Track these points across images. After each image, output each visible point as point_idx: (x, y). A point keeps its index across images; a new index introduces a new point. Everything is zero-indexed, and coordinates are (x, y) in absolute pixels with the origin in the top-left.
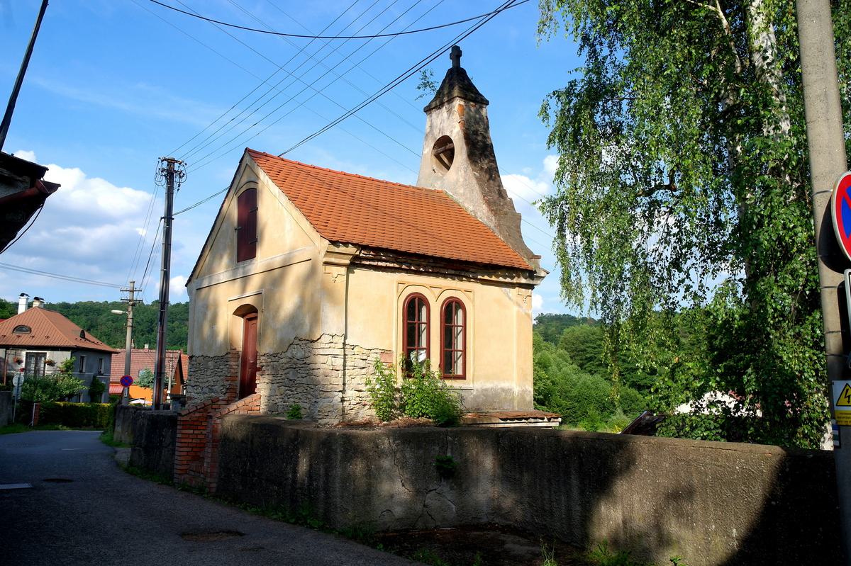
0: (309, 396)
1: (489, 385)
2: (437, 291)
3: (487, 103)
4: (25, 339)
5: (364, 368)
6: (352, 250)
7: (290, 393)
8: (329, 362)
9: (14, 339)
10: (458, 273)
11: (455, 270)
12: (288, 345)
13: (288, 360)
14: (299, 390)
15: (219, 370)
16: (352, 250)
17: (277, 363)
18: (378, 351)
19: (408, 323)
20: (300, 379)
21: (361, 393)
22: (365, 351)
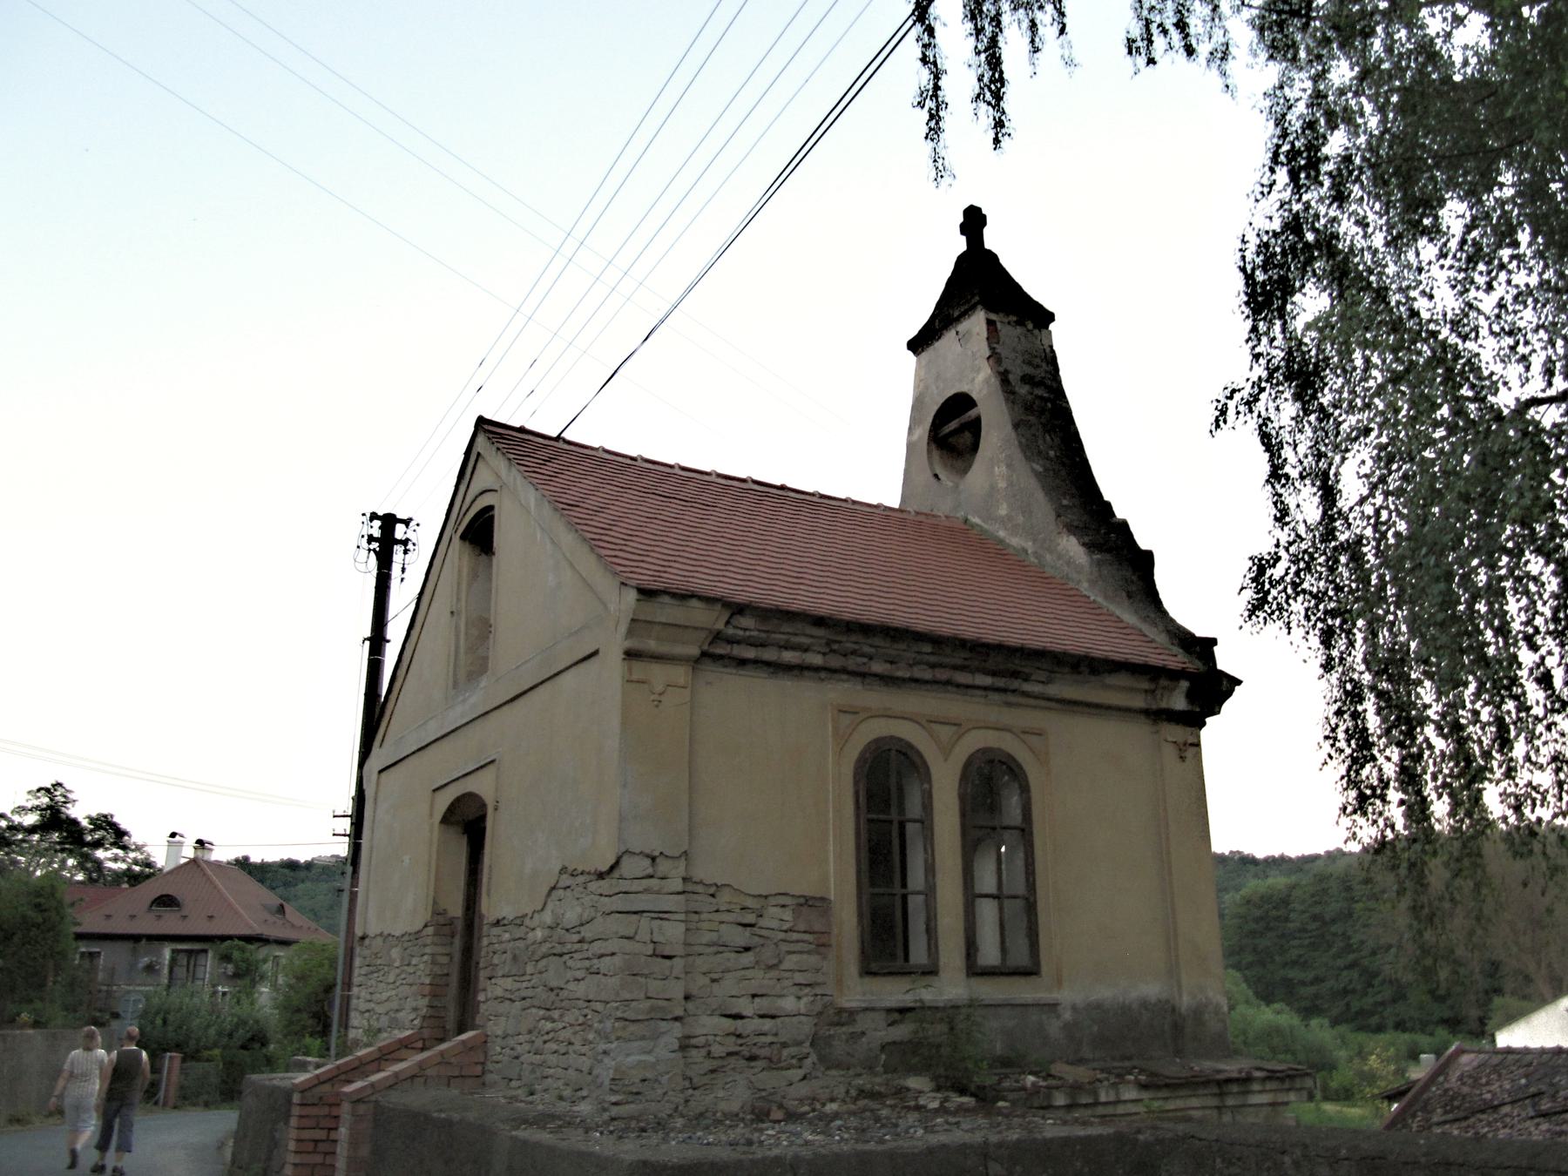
0: (591, 1036)
1: (1105, 993)
2: (945, 732)
3: (1050, 317)
4: (170, 923)
5: (747, 949)
6: (714, 619)
7: (549, 1026)
8: (644, 935)
9: (148, 924)
10: (1000, 682)
11: (994, 674)
12: (545, 890)
13: (547, 932)
14: (569, 1018)
15: (411, 969)
16: (714, 619)
17: (520, 944)
18: (787, 900)
19: (870, 821)
20: (572, 986)
21: (739, 1022)
22: (749, 903)
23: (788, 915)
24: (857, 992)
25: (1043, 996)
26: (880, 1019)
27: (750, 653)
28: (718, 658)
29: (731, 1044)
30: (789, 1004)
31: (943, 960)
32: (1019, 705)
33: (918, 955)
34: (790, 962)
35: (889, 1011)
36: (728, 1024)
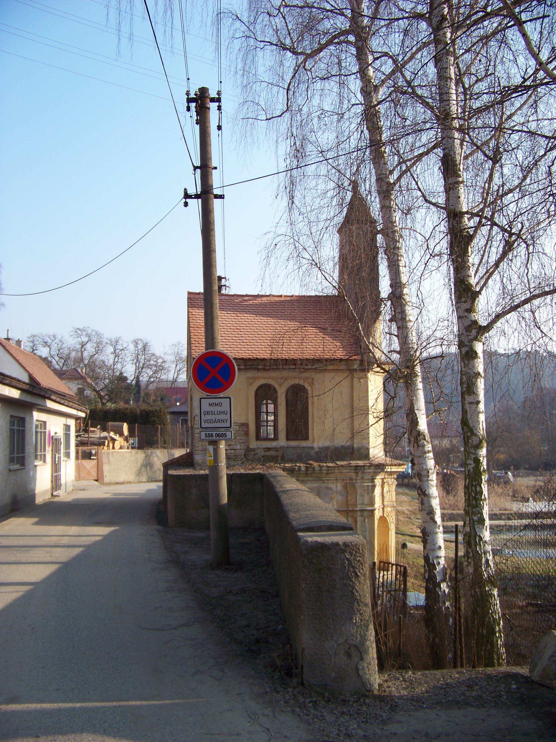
23: (237, 427)
30: (238, 447)
35: (264, 449)
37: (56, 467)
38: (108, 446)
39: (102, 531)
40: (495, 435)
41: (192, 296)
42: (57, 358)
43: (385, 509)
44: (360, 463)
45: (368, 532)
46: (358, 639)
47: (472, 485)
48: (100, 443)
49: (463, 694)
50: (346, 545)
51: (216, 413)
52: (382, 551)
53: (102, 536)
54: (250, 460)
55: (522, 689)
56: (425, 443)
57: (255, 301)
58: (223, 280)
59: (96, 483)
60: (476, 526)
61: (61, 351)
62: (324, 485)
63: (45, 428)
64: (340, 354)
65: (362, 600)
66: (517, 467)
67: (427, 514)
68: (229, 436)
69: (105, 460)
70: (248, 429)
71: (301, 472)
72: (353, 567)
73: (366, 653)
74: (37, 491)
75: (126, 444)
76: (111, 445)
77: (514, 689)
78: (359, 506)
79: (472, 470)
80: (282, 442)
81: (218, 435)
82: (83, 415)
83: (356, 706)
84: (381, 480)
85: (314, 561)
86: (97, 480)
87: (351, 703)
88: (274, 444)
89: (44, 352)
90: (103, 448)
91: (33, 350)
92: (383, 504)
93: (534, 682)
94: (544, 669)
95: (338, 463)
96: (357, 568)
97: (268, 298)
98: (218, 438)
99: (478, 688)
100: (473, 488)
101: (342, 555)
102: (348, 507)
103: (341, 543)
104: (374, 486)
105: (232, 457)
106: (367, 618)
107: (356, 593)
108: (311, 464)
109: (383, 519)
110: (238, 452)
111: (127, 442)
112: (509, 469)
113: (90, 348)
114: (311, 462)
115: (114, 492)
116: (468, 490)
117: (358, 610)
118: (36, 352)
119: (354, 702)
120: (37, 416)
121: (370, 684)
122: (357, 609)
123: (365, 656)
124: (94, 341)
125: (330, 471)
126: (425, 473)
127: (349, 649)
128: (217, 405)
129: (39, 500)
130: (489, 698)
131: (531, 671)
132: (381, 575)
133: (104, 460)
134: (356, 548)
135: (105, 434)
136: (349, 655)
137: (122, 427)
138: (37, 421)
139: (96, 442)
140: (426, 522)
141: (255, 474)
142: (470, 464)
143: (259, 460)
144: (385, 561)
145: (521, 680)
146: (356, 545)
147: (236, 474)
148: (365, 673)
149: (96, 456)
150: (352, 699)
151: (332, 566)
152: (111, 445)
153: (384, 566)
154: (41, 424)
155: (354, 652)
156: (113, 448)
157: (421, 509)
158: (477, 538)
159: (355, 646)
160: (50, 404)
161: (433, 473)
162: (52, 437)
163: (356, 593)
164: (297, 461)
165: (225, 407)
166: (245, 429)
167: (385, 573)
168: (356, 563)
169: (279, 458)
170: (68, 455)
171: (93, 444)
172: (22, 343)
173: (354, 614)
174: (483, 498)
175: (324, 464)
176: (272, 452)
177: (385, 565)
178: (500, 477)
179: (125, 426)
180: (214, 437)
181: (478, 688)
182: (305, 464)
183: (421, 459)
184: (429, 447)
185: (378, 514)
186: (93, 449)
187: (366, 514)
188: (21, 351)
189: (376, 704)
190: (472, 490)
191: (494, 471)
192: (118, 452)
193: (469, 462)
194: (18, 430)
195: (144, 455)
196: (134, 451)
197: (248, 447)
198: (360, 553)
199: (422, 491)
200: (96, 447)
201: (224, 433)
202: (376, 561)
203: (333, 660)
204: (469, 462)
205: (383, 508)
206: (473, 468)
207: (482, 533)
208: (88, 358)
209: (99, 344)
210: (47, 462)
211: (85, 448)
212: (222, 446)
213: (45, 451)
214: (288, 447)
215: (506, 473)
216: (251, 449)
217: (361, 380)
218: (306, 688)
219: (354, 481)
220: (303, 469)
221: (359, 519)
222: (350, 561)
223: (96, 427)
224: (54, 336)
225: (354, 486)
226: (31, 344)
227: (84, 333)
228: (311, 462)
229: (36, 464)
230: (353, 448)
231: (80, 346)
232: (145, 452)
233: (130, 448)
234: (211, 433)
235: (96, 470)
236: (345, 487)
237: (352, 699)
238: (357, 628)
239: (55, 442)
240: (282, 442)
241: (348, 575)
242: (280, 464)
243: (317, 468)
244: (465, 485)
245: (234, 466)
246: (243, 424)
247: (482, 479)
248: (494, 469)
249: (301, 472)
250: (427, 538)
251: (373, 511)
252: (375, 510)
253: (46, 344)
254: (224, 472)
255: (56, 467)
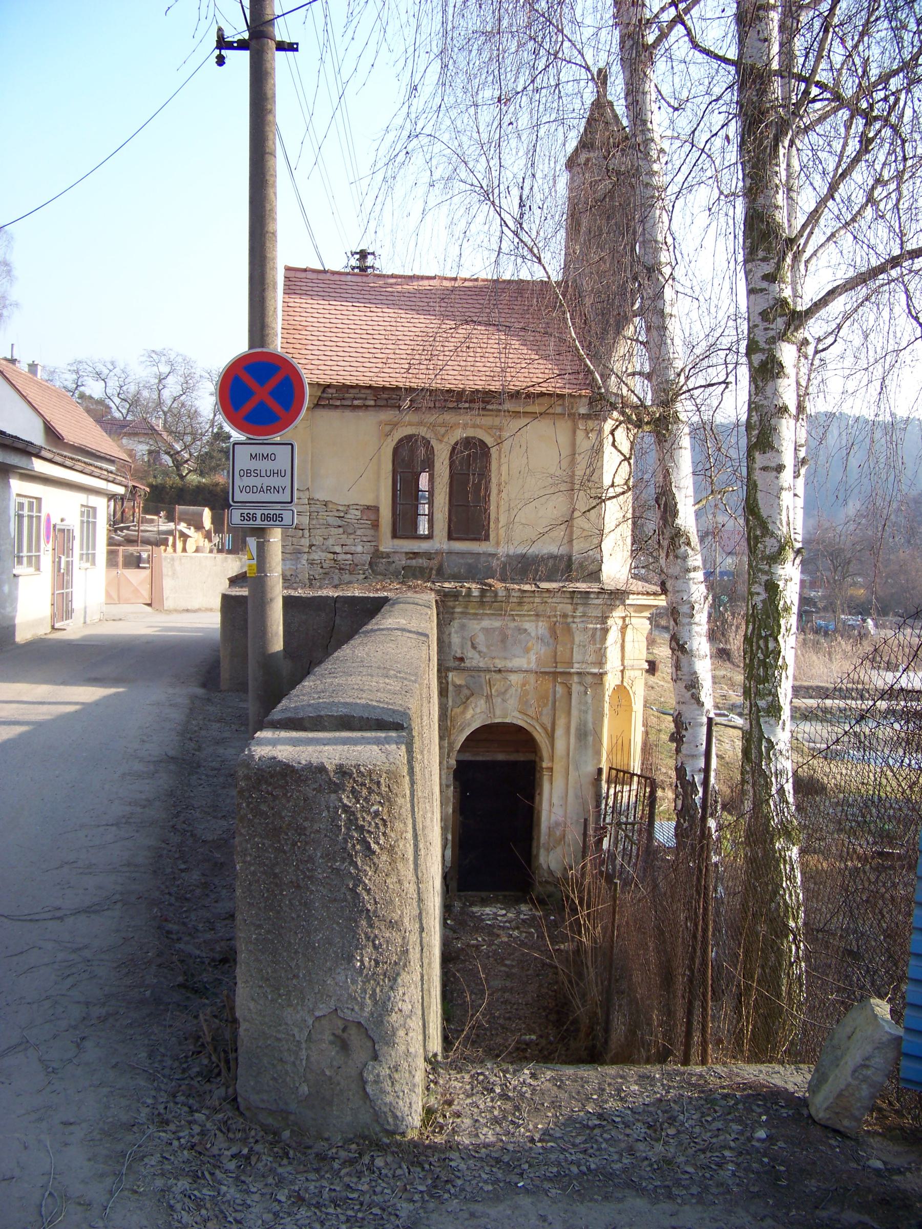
22: (341, 508)
23: (358, 513)
24: (387, 544)
25: (491, 550)
26: (403, 557)
27: (338, 403)
28: (324, 406)
29: (332, 564)
30: (359, 549)
31: (435, 533)
32: (487, 415)
33: (423, 529)
34: (359, 532)
35: (407, 553)
36: (331, 556)
37: (63, 578)
38: (174, 545)
39: (89, 694)
40: (849, 556)
41: (291, 274)
42: (117, 401)
43: (627, 673)
44: (582, 586)
45: (590, 712)
46: (367, 1009)
47: (760, 637)
48: (160, 541)
49: (631, 1151)
50: (342, 771)
51: (263, 474)
52: (614, 749)
53: (83, 704)
54: (380, 574)
55: (781, 1144)
56: (690, 552)
57: (405, 287)
58: (370, 257)
59: (148, 609)
60: (762, 720)
61: (124, 388)
62: (512, 625)
63: (39, 511)
64: (555, 386)
65: (381, 913)
66: (883, 611)
67: (686, 687)
68: (287, 520)
69: (166, 569)
70: (378, 517)
71: (472, 599)
72: (361, 829)
73: (387, 1044)
74: (18, 621)
75: (207, 545)
76: (179, 545)
77: (759, 1140)
78: (576, 665)
79: (760, 606)
80: (440, 543)
81: (266, 517)
82: (121, 490)
83: (347, 1174)
84: (620, 622)
85: (264, 808)
86: (150, 605)
87: (336, 1165)
88: (424, 546)
89: (95, 389)
90: (165, 550)
91: (78, 386)
92: (623, 664)
93: (814, 1121)
94: (840, 1095)
95: (544, 585)
96: (369, 832)
97: (432, 282)
98: (266, 523)
99: (672, 1131)
100: (761, 643)
101: (333, 796)
102: (556, 667)
103: (329, 767)
104: (606, 631)
105: (348, 567)
106: (395, 958)
107: (364, 894)
108: (490, 586)
109: (621, 689)
110: (358, 559)
111: (210, 540)
112: (869, 615)
113: (172, 388)
114: (490, 581)
115: (161, 625)
116: (752, 646)
117: (368, 938)
118: (81, 389)
119: (343, 1164)
120: (17, 486)
121: (395, 1117)
122: (366, 934)
123: (383, 1050)
124: (181, 373)
125: (525, 600)
126: (684, 609)
127: (344, 1030)
128: (266, 457)
129: (21, 636)
130: (690, 1169)
131: (814, 1087)
132: (612, 791)
133: (165, 570)
134: (371, 780)
135: (171, 526)
136: (344, 1046)
137: (201, 515)
138: (18, 495)
139: (152, 539)
140: (683, 703)
141: (320, 597)
142: (758, 594)
143: (396, 574)
144: (619, 768)
145: (784, 1112)
146: (370, 772)
147: (342, 597)
148: (383, 1092)
149: (148, 562)
150: (343, 1154)
151: (307, 824)
152: (179, 545)
153: (617, 776)
154: (88, 511)
155: (355, 1038)
156: (184, 550)
157: (674, 677)
158: (764, 744)
159: (359, 1023)
160: (39, 466)
161: (701, 611)
162: (55, 526)
163: (364, 894)
164: (466, 578)
165: (282, 462)
166: (373, 517)
167: (619, 788)
168: (369, 818)
169: (434, 572)
170: (90, 558)
171: (147, 542)
172: (39, 368)
173: (357, 948)
174: (780, 662)
175: (516, 587)
176: (420, 561)
177: (621, 776)
178: (853, 627)
179: (207, 514)
180: (259, 521)
181: (672, 1131)
182: (481, 584)
183: (680, 581)
184: (696, 560)
185: (611, 681)
186: (146, 551)
187: (589, 679)
188: (37, 383)
189: (399, 1172)
190: (759, 647)
191: (843, 616)
192: (191, 557)
193: (756, 588)
194: (29, 516)
195: (238, 563)
196: (221, 556)
197: (377, 550)
198: (379, 794)
199: (678, 644)
200: (150, 547)
201: (278, 512)
202: (604, 766)
203: (303, 1054)
204: (756, 588)
205: (622, 671)
206: (763, 601)
207: (775, 735)
208: (169, 402)
209: (187, 378)
210: (42, 569)
211: (132, 549)
212: (276, 537)
213: (38, 550)
214: (450, 553)
215: (864, 621)
216: (382, 553)
217: (590, 435)
218: (242, 1114)
219: (570, 620)
220: (476, 593)
221: (576, 688)
222: (353, 813)
223: (157, 513)
224: (112, 363)
225: (568, 630)
226: (75, 376)
227: (163, 359)
228: (490, 581)
229: (15, 572)
230: (570, 558)
231: (157, 381)
232: (240, 559)
233: (215, 551)
234: (252, 512)
235: (149, 586)
236: (553, 630)
237: (343, 1154)
238: (367, 980)
239: (62, 538)
240: (440, 543)
241: (345, 849)
242: (433, 582)
243: (502, 593)
244: (745, 635)
245: (350, 582)
246: (368, 508)
247: (779, 626)
248: (843, 612)
249: (472, 599)
250: (684, 733)
251: (601, 675)
252: (606, 673)
253: (99, 376)
254: (277, 593)
255: (63, 578)
